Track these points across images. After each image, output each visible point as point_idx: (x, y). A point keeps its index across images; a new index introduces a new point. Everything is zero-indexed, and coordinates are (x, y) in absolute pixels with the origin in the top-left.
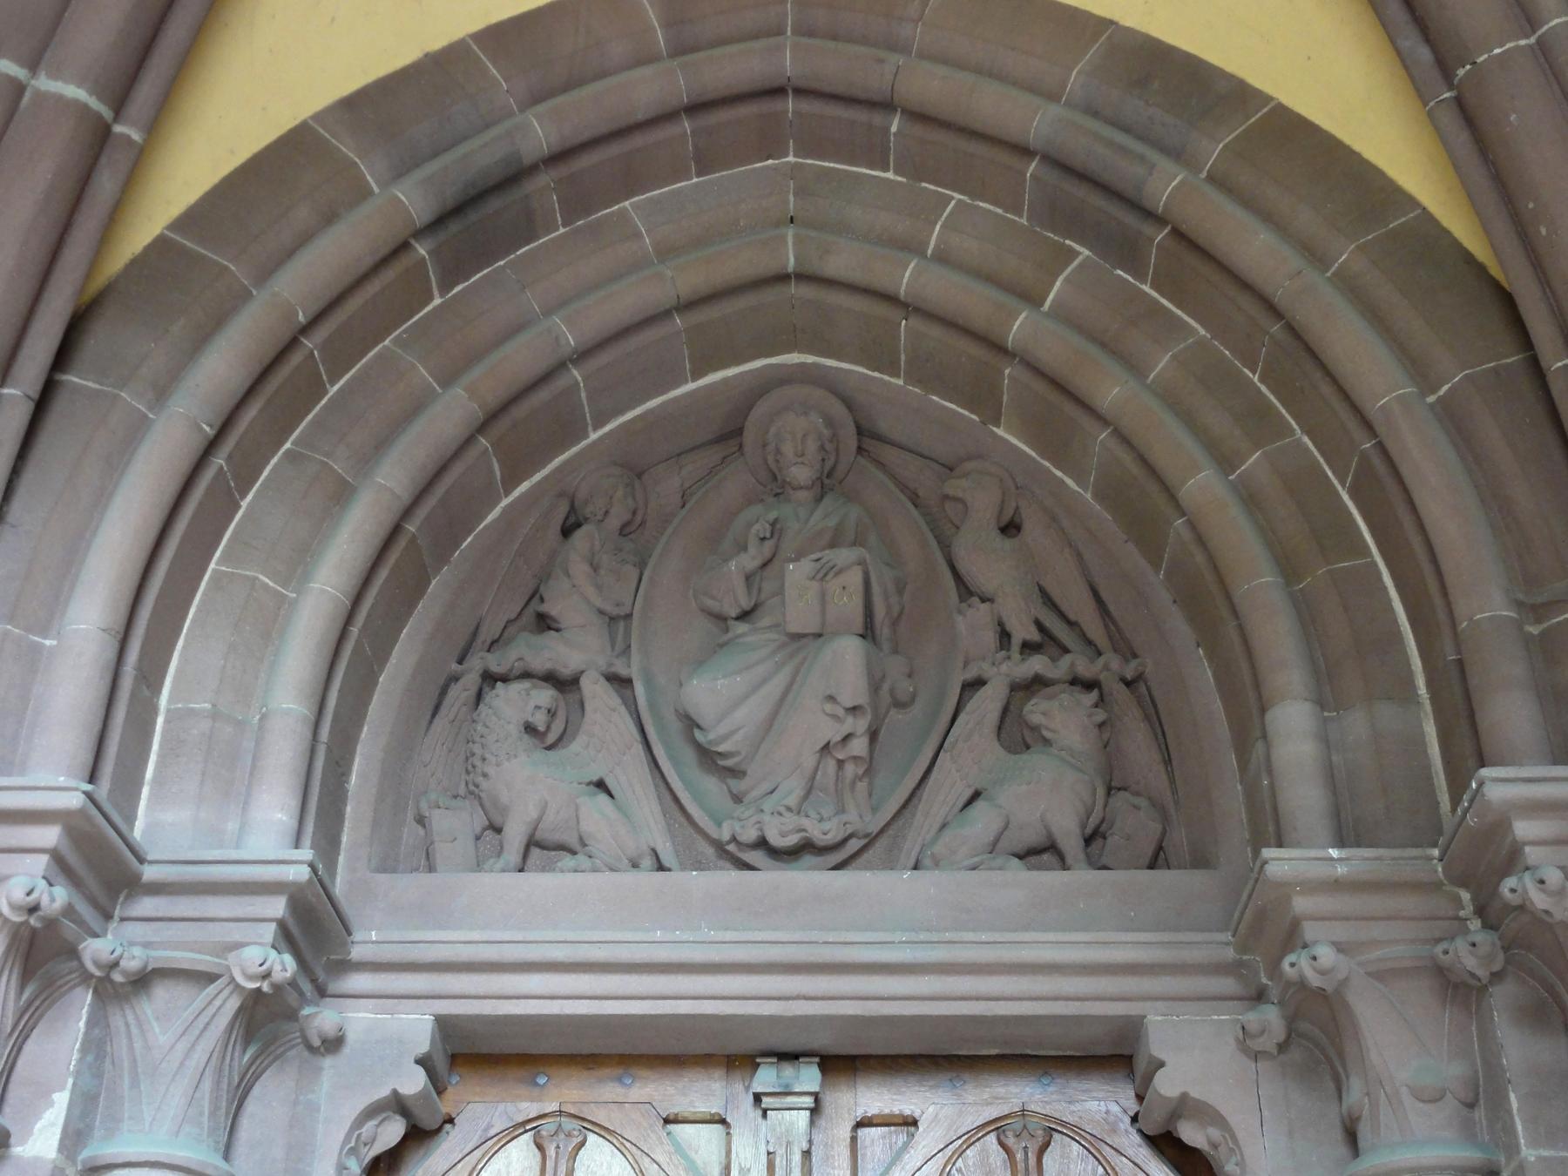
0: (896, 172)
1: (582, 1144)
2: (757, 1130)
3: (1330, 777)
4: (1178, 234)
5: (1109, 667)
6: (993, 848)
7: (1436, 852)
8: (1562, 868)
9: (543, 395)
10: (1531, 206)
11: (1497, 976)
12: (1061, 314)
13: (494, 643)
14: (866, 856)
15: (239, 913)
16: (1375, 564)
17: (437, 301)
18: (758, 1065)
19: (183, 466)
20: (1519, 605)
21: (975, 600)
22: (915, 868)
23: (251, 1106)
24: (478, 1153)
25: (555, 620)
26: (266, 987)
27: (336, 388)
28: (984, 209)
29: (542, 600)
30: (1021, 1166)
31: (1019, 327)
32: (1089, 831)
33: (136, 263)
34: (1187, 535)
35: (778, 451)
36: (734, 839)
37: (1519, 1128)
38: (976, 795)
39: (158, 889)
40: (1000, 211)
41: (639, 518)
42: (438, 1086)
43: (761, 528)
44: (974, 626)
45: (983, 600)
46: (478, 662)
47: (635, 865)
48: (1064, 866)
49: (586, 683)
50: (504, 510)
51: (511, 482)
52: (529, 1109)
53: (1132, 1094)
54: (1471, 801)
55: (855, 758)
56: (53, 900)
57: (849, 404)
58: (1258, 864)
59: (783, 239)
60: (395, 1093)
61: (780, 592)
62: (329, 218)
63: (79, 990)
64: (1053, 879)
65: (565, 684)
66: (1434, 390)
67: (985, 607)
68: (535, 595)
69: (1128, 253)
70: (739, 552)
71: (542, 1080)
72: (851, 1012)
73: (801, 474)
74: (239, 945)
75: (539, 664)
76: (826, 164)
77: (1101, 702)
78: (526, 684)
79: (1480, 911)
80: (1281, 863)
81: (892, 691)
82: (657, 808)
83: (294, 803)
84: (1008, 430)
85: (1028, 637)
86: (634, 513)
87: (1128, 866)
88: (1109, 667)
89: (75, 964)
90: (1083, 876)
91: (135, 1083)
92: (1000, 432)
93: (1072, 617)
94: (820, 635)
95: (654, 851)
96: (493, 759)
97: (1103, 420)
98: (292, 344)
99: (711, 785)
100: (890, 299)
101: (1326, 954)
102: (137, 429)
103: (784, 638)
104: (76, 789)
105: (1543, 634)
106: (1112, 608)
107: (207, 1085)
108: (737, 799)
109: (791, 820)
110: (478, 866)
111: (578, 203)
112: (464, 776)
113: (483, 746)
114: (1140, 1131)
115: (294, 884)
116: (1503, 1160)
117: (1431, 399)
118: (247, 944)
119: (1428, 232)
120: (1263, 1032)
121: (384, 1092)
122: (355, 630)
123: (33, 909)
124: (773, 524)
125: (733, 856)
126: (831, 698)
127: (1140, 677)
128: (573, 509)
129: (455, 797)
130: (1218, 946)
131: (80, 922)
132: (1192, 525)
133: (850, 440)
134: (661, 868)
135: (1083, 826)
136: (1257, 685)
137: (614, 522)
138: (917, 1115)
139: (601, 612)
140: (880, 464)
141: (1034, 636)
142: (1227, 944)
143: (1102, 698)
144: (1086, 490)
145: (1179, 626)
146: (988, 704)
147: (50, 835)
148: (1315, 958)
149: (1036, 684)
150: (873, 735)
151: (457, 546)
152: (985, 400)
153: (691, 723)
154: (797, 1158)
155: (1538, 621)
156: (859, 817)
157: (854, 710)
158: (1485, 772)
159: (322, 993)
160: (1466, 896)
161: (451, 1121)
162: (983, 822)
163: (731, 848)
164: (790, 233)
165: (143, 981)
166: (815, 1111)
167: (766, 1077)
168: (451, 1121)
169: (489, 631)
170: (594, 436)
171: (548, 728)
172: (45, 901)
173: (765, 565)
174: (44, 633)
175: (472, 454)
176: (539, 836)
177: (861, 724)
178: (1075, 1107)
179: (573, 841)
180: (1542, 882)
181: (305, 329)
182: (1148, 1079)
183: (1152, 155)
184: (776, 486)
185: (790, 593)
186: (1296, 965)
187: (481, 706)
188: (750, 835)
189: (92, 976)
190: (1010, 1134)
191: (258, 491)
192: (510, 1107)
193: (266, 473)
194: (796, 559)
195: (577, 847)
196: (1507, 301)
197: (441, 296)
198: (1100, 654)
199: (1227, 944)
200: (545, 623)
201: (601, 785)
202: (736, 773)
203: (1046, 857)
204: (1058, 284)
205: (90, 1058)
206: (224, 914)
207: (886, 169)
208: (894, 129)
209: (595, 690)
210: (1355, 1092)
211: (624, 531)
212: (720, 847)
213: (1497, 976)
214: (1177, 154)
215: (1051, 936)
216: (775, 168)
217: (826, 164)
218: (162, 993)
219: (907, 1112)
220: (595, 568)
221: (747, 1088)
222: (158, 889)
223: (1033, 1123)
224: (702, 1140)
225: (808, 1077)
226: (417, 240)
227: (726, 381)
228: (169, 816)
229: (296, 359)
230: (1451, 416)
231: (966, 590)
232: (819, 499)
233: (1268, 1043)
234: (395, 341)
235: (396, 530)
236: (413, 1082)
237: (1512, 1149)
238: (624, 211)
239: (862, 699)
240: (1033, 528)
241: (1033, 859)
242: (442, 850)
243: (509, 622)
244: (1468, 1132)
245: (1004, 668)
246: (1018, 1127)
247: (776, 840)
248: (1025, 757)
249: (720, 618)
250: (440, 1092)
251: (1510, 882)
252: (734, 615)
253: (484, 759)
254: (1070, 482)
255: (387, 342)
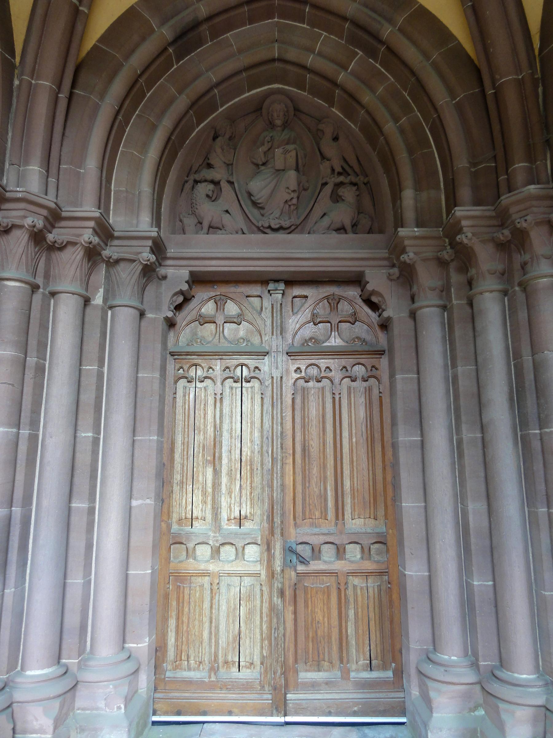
0: (307, 25)
1: (226, 302)
2: (269, 299)
3: (416, 210)
4: (389, 48)
5: (360, 179)
6: (328, 228)
7: (441, 229)
8: (472, 233)
9: (206, 98)
10: (489, 42)
11: (452, 260)
12: (353, 73)
13: (196, 171)
14: (296, 230)
15: (140, 244)
16: (433, 151)
17: (175, 67)
18: (269, 283)
19: (111, 119)
20: (470, 163)
21: (325, 160)
22: (309, 233)
23: (146, 293)
24: (201, 304)
25: (213, 166)
26: (149, 263)
27: (149, 94)
28: (332, 38)
29: (208, 159)
30: (333, 307)
31: (342, 77)
32: (353, 224)
33: (88, 53)
34: (384, 142)
35: (272, 115)
36: (262, 226)
37: (453, 296)
38: (325, 214)
39: (119, 238)
40: (337, 39)
41: (233, 136)
42: (190, 287)
43: (268, 138)
44: (325, 168)
45: (328, 160)
46: (192, 177)
47: (237, 233)
48: (346, 233)
49: (221, 183)
50: (197, 133)
51: (198, 124)
52: (212, 294)
53: (360, 290)
54: (452, 216)
55: (294, 204)
56: (95, 241)
57: (292, 100)
58: (396, 232)
59: (274, 47)
60: (181, 290)
61: (274, 157)
62: (143, 39)
63: (102, 264)
64: (343, 236)
65: (216, 183)
66: (455, 100)
67: (328, 162)
68: (207, 158)
69: (372, 53)
70: (262, 146)
71: (215, 287)
72: (293, 270)
73: (278, 122)
74: (140, 253)
75: (209, 177)
76: (287, 22)
77: (358, 189)
78: (206, 184)
79: (450, 244)
80: (402, 232)
81: (303, 186)
82: (242, 218)
83: (150, 216)
84: (336, 109)
85: (339, 171)
86: (232, 133)
87: (364, 233)
88: (360, 179)
89: (100, 257)
90: (351, 236)
91: (118, 287)
92: (334, 110)
93: (351, 165)
94: (284, 170)
95: (242, 229)
96: (199, 204)
97: (363, 107)
98: (136, 81)
99: (256, 212)
100: (304, 67)
101: (411, 255)
102: (97, 107)
103: (274, 171)
104: (97, 212)
105: (476, 171)
106: (362, 163)
107: (136, 287)
108: (263, 215)
109: (277, 221)
110: (197, 233)
111: (215, 34)
112: (191, 209)
113: (196, 200)
114: (362, 299)
115: (153, 237)
116: (448, 304)
117: (454, 102)
118: (143, 253)
119: (459, 47)
120: (393, 275)
121: (178, 289)
122: (160, 168)
123: (90, 243)
124: (271, 137)
125: (261, 230)
126: (288, 188)
127: (368, 182)
128: (215, 132)
129: (189, 214)
130: (384, 253)
131: (100, 246)
132: (385, 139)
133: (292, 112)
134: (244, 233)
135: (352, 223)
136: (400, 185)
137: (227, 136)
138: (308, 295)
139: (225, 163)
140: (300, 120)
141: (340, 170)
142: (386, 253)
143: (358, 188)
144: (357, 128)
145: (380, 169)
146: (328, 189)
147: (92, 224)
148: (408, 256)
149: (342, 184)
150: (298, 198)
151: (185, 143)
152: (330, 100)
153: (250, 195)
154: (279, 305)
155: (474, 167)
156: (294, 220)
157: (294, 191)
158: (456, 208)
159: (160, 265)
160: (447, 240)
161: (194, 297)
162: (326, 221)
163: (261, 228)
164: (276, 45)
165: (117, 261)
166: (283, 294)
167: (271, 286)
168: (194, 297)
169: (194, 169)
170: (220, 110)
171: (212, 196)
172: (93, 241)
173: (269, 149)
174: (80, 168)
175: (188, 116)
176: (212, 225)
177: (295, 195)
178: (347, 293)
179: (221, 227)
180: (467, 236)
181: (140, 76)
182: (365, 286)
183: (383, 22)
184: (271, 125)
185: (276, 158)
186: (404, 258)
187: (194, 190)
188: (267, 225)
189: (105, 260)
190: (330, 299)
191: (130, 126)
192: (208, 293)
193: (132, 121)
194: (278, 148)
195: (222, 228)
196: (478, 71)
197: (176, 65)
198: (358, 175)
199: (386, 253)
200: (210, 166)
201: (227, 211)
202: (263, 208)
203: (342, 231)
204: (353, 63)
205: (107, 281)
206: (136, 245)
207: (304, 24)
208: (307, 10)
209: (224, 185)
210: (415, 289)
211: (230, 138)
212: (258, 228)
213: (452, 260)
214: (390, 21)
215: (343, 251)
216: (271, 23)
217: (287, 22)
218: (122, 265)
219: (305, 294)
220: (223, 150)
221: (266, 289)
222: (119, 238)
223: (336, 297)
224: (256, 301)
225: (282, 286)
226: (169, 46)
227: (257, 93)
228: (119, 219)
229: (138, 86)
230: (459, 107)
231: (323, 157)
232: (283, 130)
233: (395, 277)
234: (164, 79)
235: (169, 139)
236: (185, 287)
237: (450, 301)
238: (227, 37)
239: (296, 188)
240: (341, 140)
241: (338, 231)
242: (187, 228)
243: (200, 166)
244: (441, 298)
245: (333, 179)
246: (332, 298)
247: (273, 226)
248: (338, 204)
249: (257, 165)
250: (191, 289)
251: (459, 237)
252: (260, 164)
253: (196, 204)
254: (352, 125)
255: (162, 80)
